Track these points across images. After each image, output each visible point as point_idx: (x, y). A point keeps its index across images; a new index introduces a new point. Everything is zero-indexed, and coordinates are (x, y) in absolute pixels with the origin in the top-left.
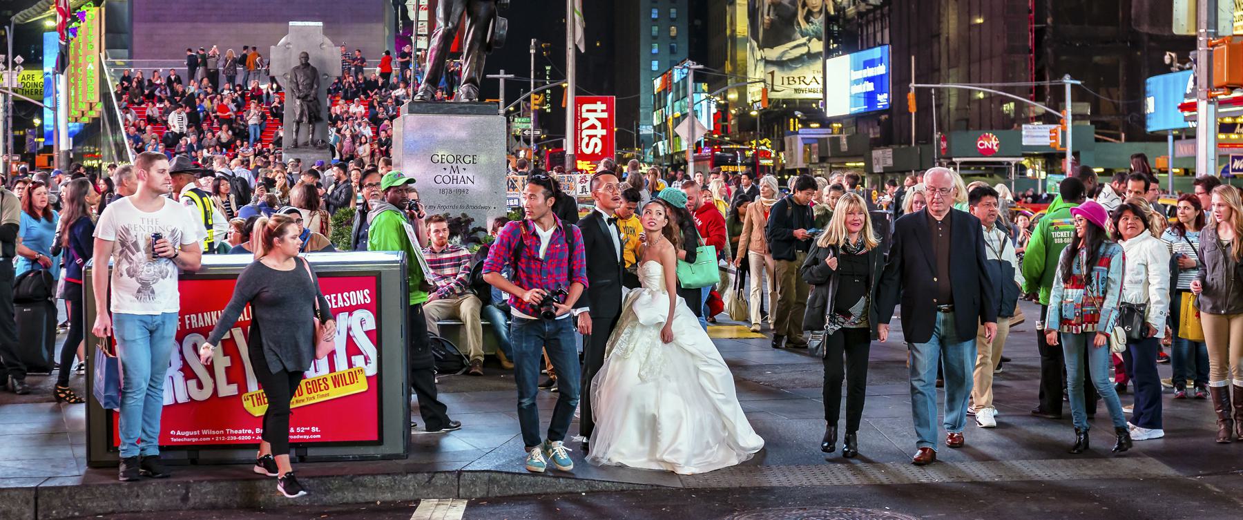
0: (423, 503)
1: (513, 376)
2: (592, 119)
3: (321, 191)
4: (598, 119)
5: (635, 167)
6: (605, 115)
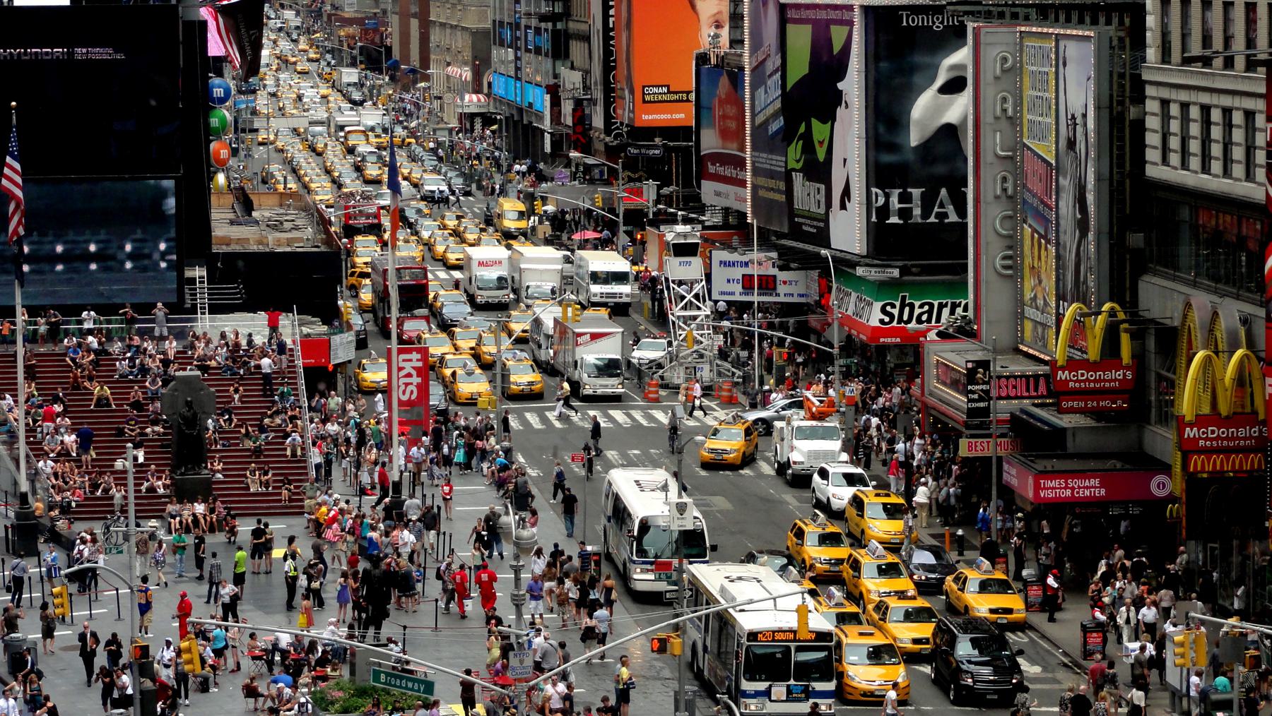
0: (743, 442)
1: (1206, 410)
2: (408, 368)
3: (365, 250)
5: (64, 455)
6: (420, 364)
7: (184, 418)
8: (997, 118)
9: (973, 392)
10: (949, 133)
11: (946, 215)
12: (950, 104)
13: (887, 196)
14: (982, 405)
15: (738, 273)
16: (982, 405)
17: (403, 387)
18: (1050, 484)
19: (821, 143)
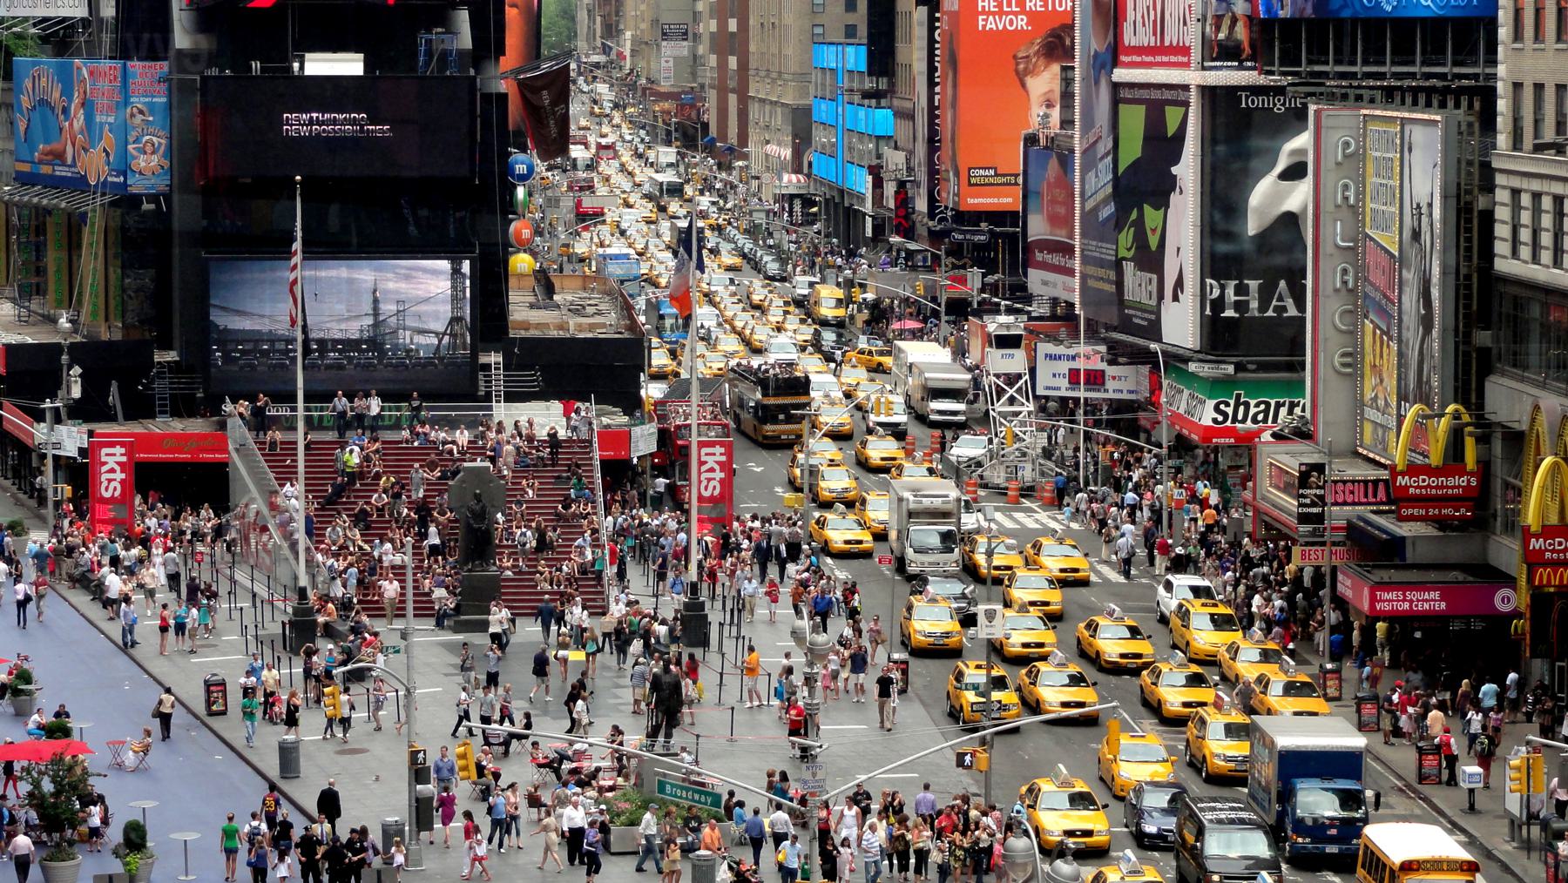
2: (711, 462)
4: (717, 463)
6: (723, 458)
7: (472, 512)
8: (1338, 206)
9: (1303, 496)
10: (1290, 220)
11: (1284, 309)
12: (1289, 193)
13: (1223, 288)
14: (1315, 510)
15: (1064, 367)
16: (1315, 510)
17: (704, 483)
18: (1387, 596)
19: (1154, 231)
